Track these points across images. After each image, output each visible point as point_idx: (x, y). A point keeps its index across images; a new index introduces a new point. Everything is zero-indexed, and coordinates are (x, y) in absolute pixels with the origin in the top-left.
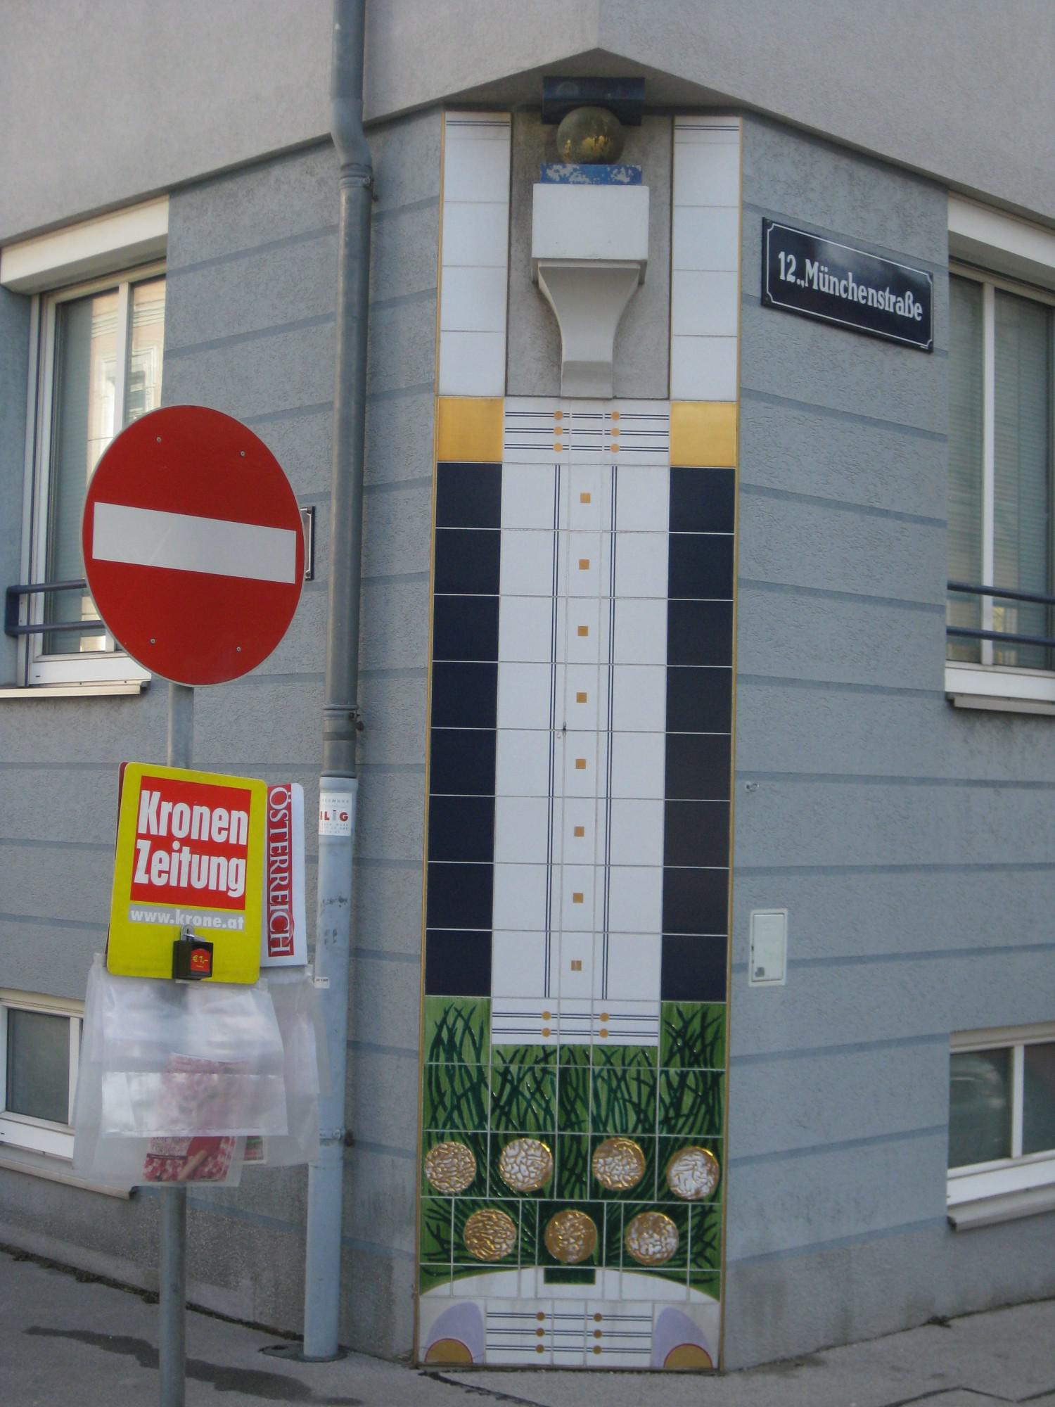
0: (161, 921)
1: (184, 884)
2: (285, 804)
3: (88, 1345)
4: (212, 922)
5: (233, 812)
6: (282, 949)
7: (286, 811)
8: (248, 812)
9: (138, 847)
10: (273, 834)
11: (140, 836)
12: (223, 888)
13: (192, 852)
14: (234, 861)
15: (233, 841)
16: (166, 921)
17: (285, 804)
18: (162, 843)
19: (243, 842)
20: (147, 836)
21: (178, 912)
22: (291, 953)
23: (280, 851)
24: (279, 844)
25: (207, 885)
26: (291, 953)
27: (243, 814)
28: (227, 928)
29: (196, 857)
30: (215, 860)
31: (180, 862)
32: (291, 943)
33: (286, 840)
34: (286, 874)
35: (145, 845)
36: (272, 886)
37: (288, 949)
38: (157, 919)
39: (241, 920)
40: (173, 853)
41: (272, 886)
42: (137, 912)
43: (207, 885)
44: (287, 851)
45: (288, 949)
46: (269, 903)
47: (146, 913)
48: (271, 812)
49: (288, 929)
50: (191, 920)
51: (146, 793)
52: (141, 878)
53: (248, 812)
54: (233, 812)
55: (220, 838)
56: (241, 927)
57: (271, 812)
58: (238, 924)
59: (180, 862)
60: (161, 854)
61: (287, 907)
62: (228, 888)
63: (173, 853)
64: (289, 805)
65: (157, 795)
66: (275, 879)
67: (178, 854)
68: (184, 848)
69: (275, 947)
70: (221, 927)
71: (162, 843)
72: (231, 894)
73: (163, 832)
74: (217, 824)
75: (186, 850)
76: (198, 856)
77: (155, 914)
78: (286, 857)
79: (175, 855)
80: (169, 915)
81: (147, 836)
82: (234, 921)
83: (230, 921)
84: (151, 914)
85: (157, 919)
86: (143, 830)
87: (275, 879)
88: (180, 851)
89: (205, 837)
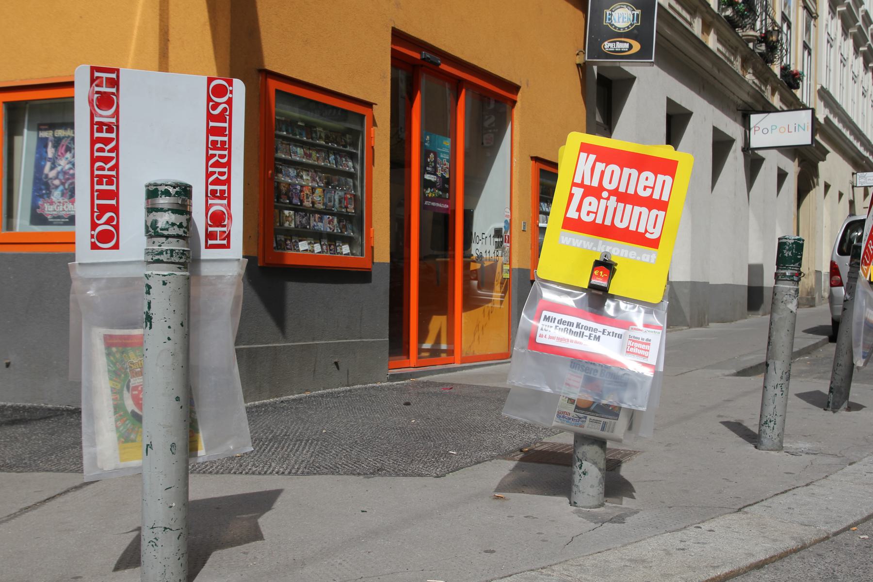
0: (574, 244)
1: (608, 222)
2: (225, 99)
3: (273, 507)
4: (620, 252)
5: (625, 169)
6: (218, 242)
7: (226, 106)
8: (673, 177)
9: (572, 192)
10: (213, 127)
11: (574, 184)
12: (641, 230)
13: (618, 201)
14: (654, 212)
15: (656, 196)
16: (590, 248)
17: (225, 99)
18: (595, 192)
19: (665, 198)
20: (581, 185)
21: (601, 242)
22: (227, 246)
23: (219, 145)
24: (219, 139)
25: (628, 227)
26: (227, 246)
27: (668, 179)
28: (641, 260)
29: (621, 205)
30: (637, 209)
31: (607, 207)
32: (228, 237)
33: (226, 136)
34: (226, 170)
35: (578, 192)
36: (210, 180)
37: (225, 242)
38: (571, 244)
39: (653, 256)
40: (601, 200)
41: (210, 180)
42: (577, 240)
43: (628, 227)
44: (226, 147)
45: (225, 242)
46: (207, 195)
47: (574, 240)
48: (211, 104)
49: (226, 223)
50: (611, 250)
51: (583, 155)
52: (573, 214)
53: (673, 177)
54: (625, 169)
55: (646, 194)
56: (652, 261)
57: (211, 104)
58: (650, 258)
59: (607, 207)
60: (592, 199)
61: (225, 202)
62: (646, 231)
63: (601, 200)
64: (230, 100)
65: (592, 157)
66: (214, 173)
67: (606, 201)
68: (611, 197)
69: (211, 239)
70: (635, 259)
71: (595, 192)
72: (648, 235)
73: (595, 183)
74: (642, 183)
75: (613, 199)
76: (639, 231)
77: (570, 239)
78: (226, 153)
79: (603, 202)
80: (592, 244)
81: (581, 185)
82: (648, 256)
83: (644, 255)
84: (566, 238)
85: (571, 244)
86: (578, 180)
87: (214, 173)
88: (608, 199)
89: (631, 191)
